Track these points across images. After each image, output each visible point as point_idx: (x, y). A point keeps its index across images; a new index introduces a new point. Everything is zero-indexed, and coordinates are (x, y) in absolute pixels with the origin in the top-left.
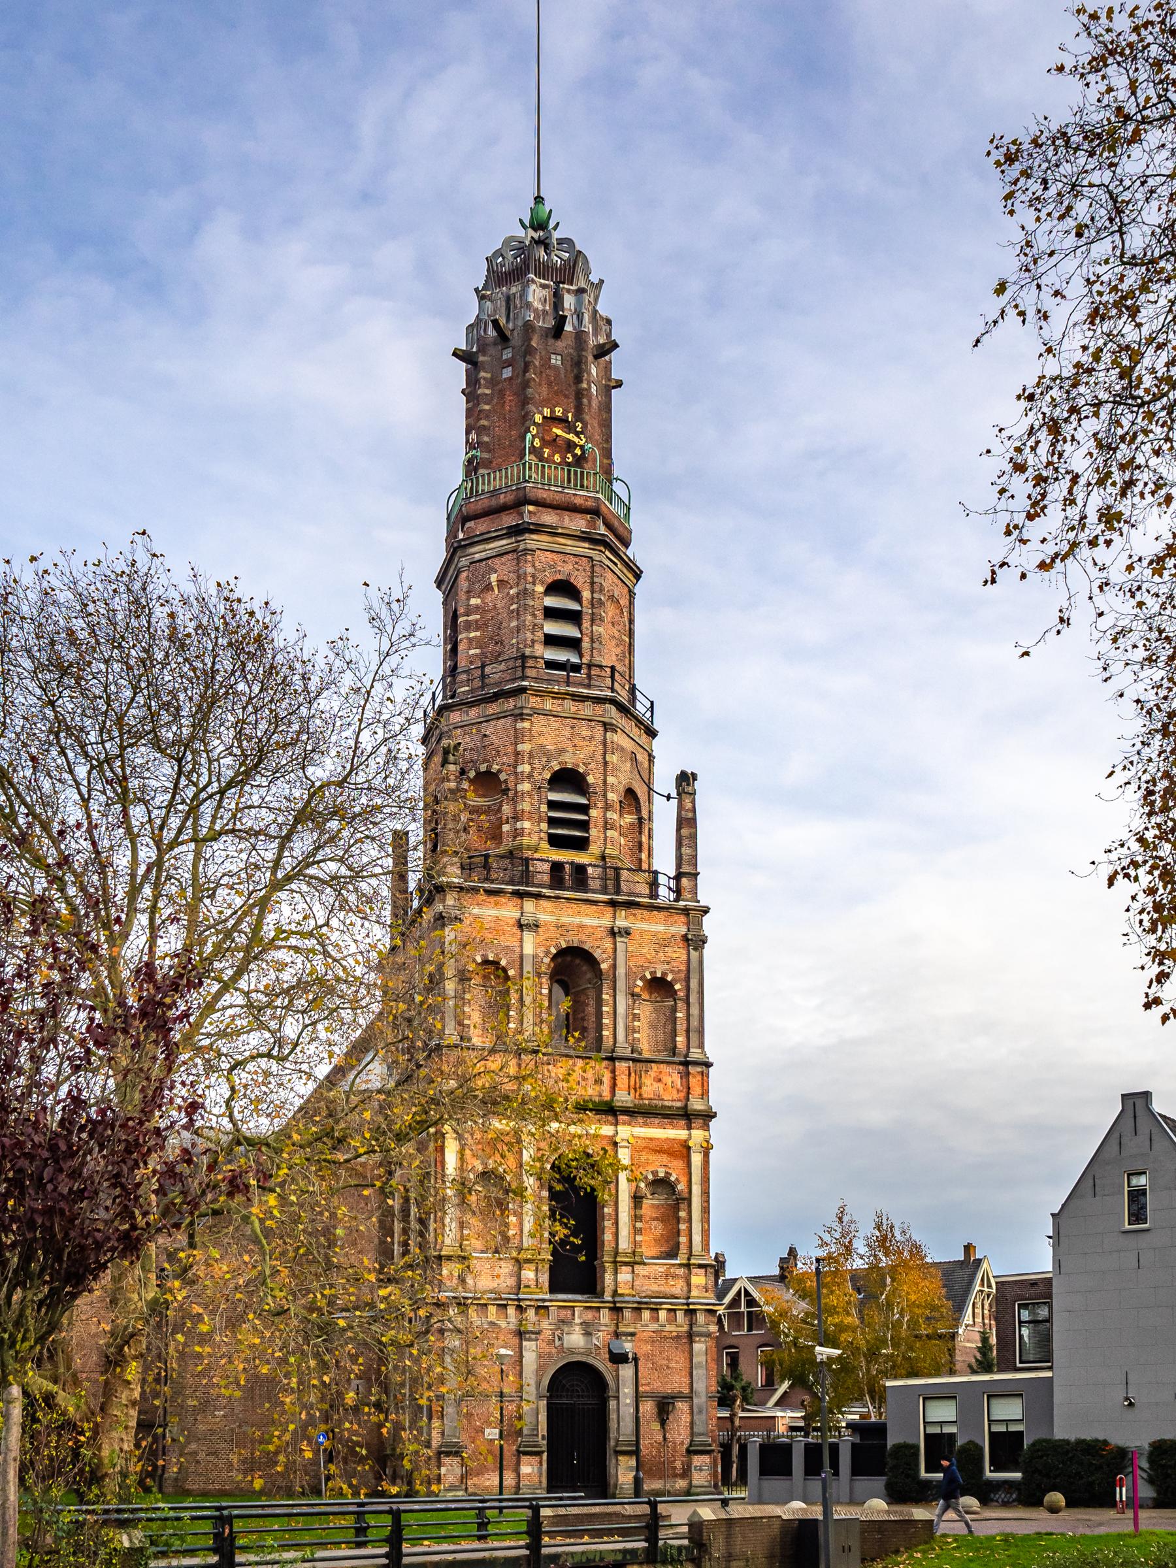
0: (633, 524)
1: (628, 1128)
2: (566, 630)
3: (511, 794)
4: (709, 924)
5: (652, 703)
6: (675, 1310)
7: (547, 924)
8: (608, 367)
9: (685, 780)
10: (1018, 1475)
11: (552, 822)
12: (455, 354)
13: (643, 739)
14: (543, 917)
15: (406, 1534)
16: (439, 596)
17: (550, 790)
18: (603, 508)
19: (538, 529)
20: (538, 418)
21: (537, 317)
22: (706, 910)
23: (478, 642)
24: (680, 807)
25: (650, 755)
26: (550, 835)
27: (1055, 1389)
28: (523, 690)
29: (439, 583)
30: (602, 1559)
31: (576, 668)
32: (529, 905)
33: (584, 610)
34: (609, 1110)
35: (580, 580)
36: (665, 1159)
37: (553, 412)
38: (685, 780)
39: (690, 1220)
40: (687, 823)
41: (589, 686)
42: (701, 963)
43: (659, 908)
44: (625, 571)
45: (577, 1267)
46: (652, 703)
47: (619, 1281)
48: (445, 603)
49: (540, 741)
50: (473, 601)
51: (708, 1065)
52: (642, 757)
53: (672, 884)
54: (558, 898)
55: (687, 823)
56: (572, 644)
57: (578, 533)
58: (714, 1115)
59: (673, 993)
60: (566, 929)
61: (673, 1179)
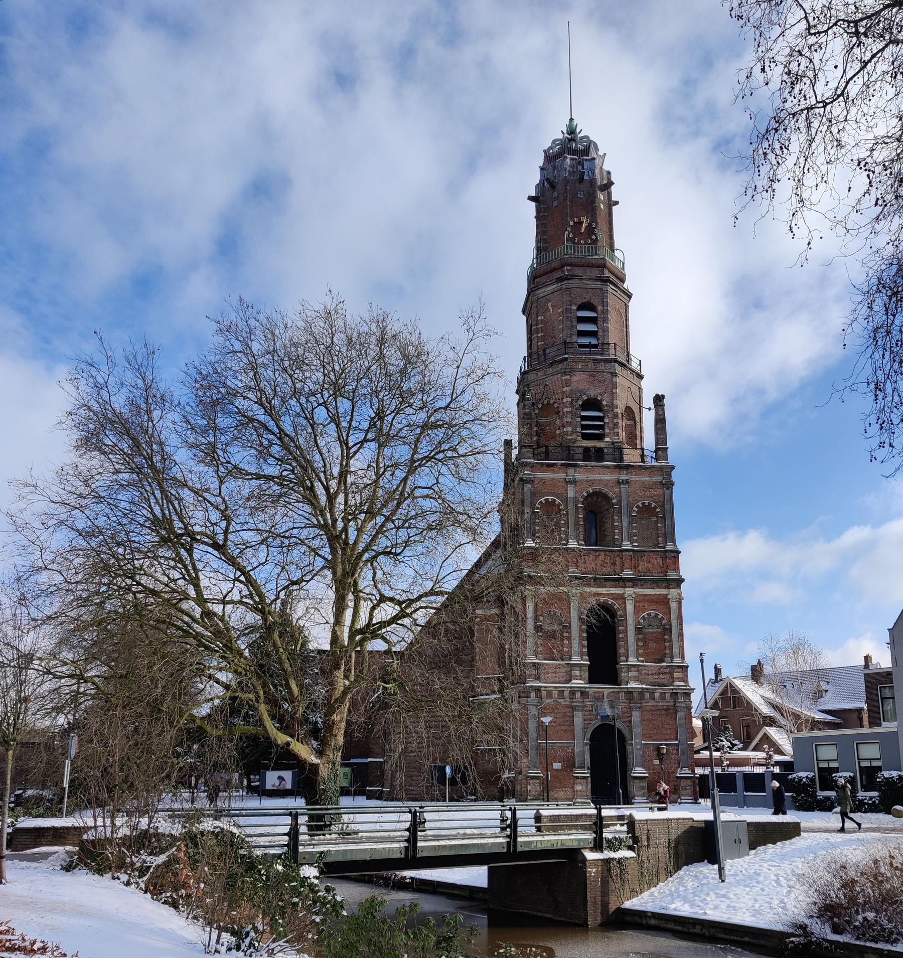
0: (626, 271)
1: (632, 589)
3: (561, 414)
7: (581, 480)
8: (609, 195)
9: (659, 400)
14: (578, 476)
15: (519, 823)
16: (524, 318)
17: (582, 410)
18: (608, 264)
19: (571, 277)
20: (572, 223)
21: (570, 175)
22: (673, 468)
23: (543, 338)
24: (656, 413)
25: (640, 388)
28: (566, 359)
29: (524, 312)
30: (562, 845)
31: (595, 346)
32: (571, 471)
36: (654, 606)
38: (659, 400)
39: (671, 641)
40: (660, 422)
41: (603, 354)
43: (645, 468)
48: (527, 321)
49: (576, 384)
50: (539, 318)
53: (653, 455)
54: (586, 466)
55: (660, 422)
56: (593, 334)
58: (683, 580)
59: (656, 514)
60: (592, 483)
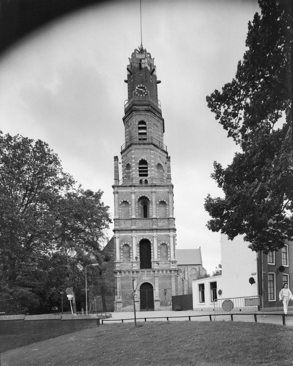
1: (118, 234)
5: (166, 146)
6: (167, 271)
7: (137, 192)
10: (5, 313)
26: (139, 174)
33: (147, 126)
34: (152, 230)
44: (158, 118)
46: (166, 146)
47: (154, 266)
56: (145, 134)
57: (144, 110)
60: (142, 192)
61: (166, 243)
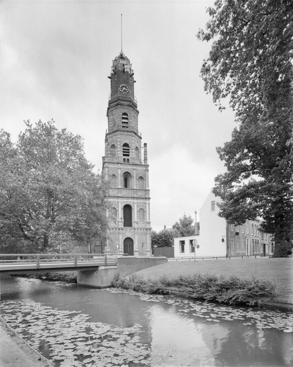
1: (136, 200)
2: (126, 121)
4: (149, 168)
9: (145, 144)
11: (123, 152)
12: (108, 77)
13: (139, 139)
20: (121, 86)
27: (21, 269)
29: (107, 116)
35: (128, 113)
37: (123, 85)
42: (148, 177)
45: (128, 222)
47: (134, 225)
51: (149, 190)
52: (139, 142)
55: (145, 152)
60: (126, 169)
